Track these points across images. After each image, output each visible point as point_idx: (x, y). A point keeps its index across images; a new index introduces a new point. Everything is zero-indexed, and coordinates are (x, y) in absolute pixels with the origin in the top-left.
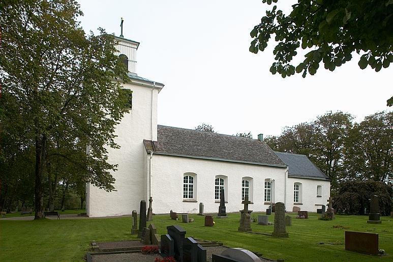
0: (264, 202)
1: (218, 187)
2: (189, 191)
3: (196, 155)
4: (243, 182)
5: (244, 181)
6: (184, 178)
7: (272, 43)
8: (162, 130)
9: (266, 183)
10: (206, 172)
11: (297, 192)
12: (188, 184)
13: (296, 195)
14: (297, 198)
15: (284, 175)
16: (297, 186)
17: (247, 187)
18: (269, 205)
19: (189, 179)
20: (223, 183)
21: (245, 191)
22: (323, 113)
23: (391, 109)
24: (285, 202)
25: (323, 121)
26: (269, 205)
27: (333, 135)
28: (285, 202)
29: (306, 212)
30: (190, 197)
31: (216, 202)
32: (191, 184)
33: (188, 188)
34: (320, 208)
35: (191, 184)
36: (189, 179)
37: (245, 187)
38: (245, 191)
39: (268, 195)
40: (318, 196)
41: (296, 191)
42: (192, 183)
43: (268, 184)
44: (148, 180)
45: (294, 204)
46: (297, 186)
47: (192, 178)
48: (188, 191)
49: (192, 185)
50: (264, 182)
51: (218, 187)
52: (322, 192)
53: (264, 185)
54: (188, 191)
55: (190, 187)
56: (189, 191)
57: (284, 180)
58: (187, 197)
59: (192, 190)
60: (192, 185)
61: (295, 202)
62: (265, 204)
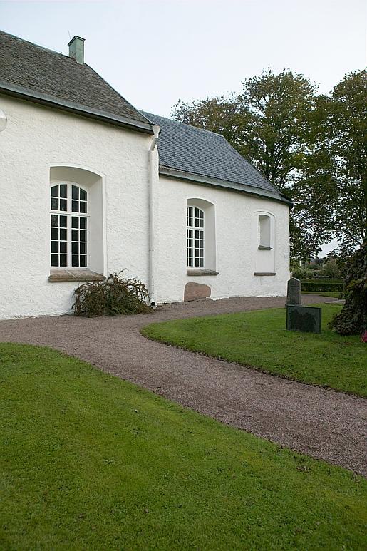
0: (48, 269)
1: (64, 219)
5: (190, 209)
6: (54, 190)
9: (190, 209)
12: (69, 214)
13: (196, 248)
14: (79, 248)
15: (141, 159)
16: (196, 213)
18: (76, 286)
22: (257, 72)
24: (150, 276)
25: (258, 89)
26: (76, 286)
27: (276, 117)
28: (150, 276)
30: (75, 263)
32: (79, 215)
35: (79, 215)
37: (194, 228)
40: (261, 248)
42: (83, 210)
45: (190, 274)
47: (202, 213)
49: (83, 220)
50: (186, 207)
52: (272, 234)
53: (185, 217)
57: (141, 184)
58: (64, 264)
60: (83, 220)
61: (194, 267)
62: (53, 279)
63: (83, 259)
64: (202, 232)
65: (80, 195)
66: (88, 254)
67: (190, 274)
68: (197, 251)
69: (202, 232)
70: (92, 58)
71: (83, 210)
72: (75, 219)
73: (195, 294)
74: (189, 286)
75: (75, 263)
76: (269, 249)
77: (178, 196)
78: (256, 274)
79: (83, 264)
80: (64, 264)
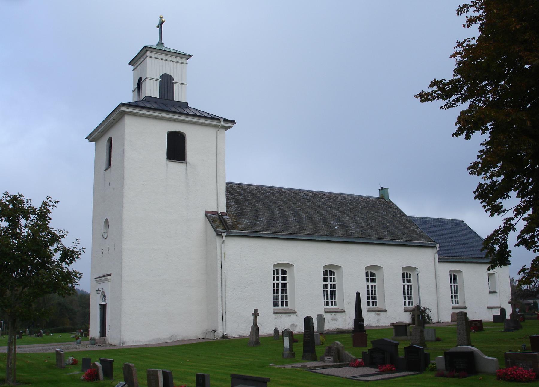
2: (281, 294)
3: (339, 237)
4: (325, 273)
7: (435, 88)
8: (233, 191)
10: (307, 259)
11: (456, 287)
13: (454, 291)
14: (333, 298)
16: (454, 276)
17: (284, 282)
19: (281, 273)
20: (334, 278)
21: (329, 289)
23: (489, 139)
29: (480, 321)
31: (275, 313)
33: (280, 289)
34: (497, 312)
36: (281, 273)
37: (329, 283)
38: (329, 289)
39: (408, 293)
40: (491, 292)
41: (453, 284)
43: (408, 274)
44: (219, 279)
45: (453, 308)
46: (455, 276)
47: (334, 273)
48: (280, 295)
49: (286, 284)
51: (331, 281)
54: (280, 295)
55: (331, 288)
56: (281, 294)
58: (278, 305)
59: (286, 293)
60: (286, 284)
61: (454, 305)
63: (286, 303)
64: (411, 286)
65: (284, 272)
66: (289, 301)
67: (453, 308)
68: (408, 297)
69: (411, 286)
70: (393, 198)
71: (286, 280)
72: (282, 284)
73: (461, 317)
74: (453, 314)
75: (283, 305)
76: (496, 292)
77: (446, 268)
78: (488, 308)
79: (286, 305)
80: (278, 305)
